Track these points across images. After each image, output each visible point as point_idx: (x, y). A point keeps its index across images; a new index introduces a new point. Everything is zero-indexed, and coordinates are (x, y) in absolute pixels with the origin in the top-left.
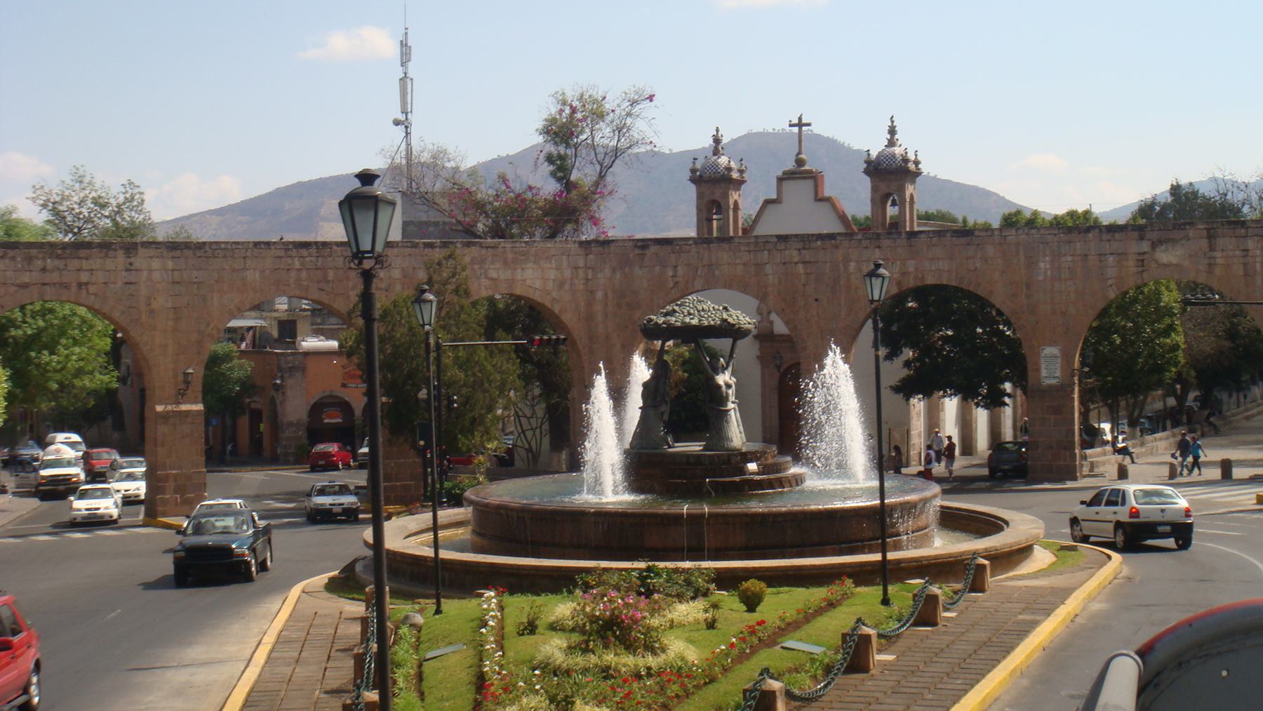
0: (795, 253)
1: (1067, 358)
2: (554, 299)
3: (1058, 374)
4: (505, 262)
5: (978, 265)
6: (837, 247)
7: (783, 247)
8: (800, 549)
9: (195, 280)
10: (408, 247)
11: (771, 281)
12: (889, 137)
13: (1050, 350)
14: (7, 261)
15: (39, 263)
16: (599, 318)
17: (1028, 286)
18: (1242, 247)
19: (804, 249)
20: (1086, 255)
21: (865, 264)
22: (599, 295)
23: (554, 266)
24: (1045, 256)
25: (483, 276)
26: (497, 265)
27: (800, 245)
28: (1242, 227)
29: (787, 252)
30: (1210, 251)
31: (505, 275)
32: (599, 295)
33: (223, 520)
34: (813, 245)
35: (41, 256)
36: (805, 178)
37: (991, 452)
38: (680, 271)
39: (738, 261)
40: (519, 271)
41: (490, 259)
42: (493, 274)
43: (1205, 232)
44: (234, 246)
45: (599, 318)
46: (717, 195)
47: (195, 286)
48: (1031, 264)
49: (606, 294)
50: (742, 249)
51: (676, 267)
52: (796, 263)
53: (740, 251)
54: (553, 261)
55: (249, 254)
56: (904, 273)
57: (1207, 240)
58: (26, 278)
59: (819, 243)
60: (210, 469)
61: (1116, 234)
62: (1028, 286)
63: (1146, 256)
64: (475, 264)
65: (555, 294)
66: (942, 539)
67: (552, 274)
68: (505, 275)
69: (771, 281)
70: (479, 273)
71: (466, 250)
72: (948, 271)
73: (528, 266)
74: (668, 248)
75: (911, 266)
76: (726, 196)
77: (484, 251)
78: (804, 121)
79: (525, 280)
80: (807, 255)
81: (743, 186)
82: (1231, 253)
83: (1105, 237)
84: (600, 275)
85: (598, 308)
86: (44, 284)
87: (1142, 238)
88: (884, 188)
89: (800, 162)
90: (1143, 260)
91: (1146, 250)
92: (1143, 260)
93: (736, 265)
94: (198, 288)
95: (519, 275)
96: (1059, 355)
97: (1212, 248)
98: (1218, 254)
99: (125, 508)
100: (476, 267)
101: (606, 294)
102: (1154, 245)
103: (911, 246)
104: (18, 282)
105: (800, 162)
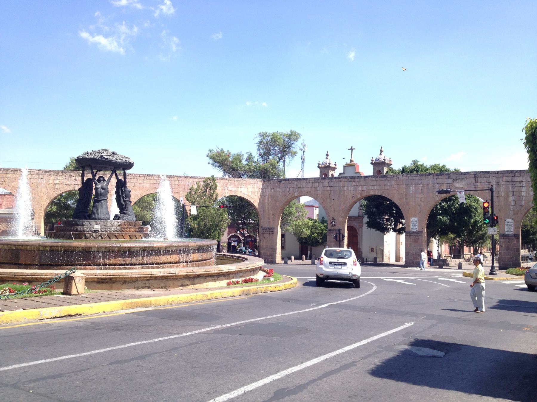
0: (327, 183)
1: (420, 222)
3: (417, 228)
4: (235, 185)
5: (388, 188)
6: (341, 181)
7: (323, 181)
8: (114, 267)
11: (319, 193)
13: (414, 219)
14: (63, 177)
15: (73, 178)
16: (266, 204)
17: (406, 195)
18: (488, 181)
19: (330, 182)
20: (428, 184)
21: (350, 187)
22: (267, 197)
23: (252, 187)
24: (412, 184)
26: (232, 186)
27: (329, 181)
28: (488, 174)
29: (324, 183)
30: (475, 182)
31: (234, 189)
32: (267, 197)
34: (333, 180)
35: (74, 175)
36: (352, 166)
38: (291, 189)
39: (309, 186)
40: (239, 188)
41: (229, 184)
42: (230, 189)
43: (473, 175)
44: (140, 175)
45: (266, 204)
46: (326, 172)
48: (408, 188)
49: (269, 197)
50: (310, 182)
51: (290, 188)
52: (327, 187)
53: (310, 183)
55: (145, 178)
56: (363, 190)
57: (474, 179)
58: (69, 182)
59: (335, 180)
61: (439, 176)
62: (406, 195)
63: (451, 185)
65: (252, 196)
67: (251, 190)
68: (234, 189)
69: (319, 193)
71: (221, 181)
72: (378, 190)
74: (288, 182)
75: (365, 188)
76: (329, 172)
77: (227, 181)
78: (353, 148)
80: (331, 184)
81: (336, 170)
82: (484, 184)
83: (435, 177)
84: (267, 191)
85: (266, 201)
86: (75, 185)
87: (449, 178)
88: (377, 169)
89: (351, 161)
90: (449, 186)
91: (450, 182)
92: (449, 186)
93: (308, 187)
95: (239, 189)
96: (417, 220)
97: (476, 182)
98: (479, 184)
100: (224, 186)
101: (269, 197)
102: (454, 181)
103: (365, 181)
104: (66, 183)
105: (351, 161)
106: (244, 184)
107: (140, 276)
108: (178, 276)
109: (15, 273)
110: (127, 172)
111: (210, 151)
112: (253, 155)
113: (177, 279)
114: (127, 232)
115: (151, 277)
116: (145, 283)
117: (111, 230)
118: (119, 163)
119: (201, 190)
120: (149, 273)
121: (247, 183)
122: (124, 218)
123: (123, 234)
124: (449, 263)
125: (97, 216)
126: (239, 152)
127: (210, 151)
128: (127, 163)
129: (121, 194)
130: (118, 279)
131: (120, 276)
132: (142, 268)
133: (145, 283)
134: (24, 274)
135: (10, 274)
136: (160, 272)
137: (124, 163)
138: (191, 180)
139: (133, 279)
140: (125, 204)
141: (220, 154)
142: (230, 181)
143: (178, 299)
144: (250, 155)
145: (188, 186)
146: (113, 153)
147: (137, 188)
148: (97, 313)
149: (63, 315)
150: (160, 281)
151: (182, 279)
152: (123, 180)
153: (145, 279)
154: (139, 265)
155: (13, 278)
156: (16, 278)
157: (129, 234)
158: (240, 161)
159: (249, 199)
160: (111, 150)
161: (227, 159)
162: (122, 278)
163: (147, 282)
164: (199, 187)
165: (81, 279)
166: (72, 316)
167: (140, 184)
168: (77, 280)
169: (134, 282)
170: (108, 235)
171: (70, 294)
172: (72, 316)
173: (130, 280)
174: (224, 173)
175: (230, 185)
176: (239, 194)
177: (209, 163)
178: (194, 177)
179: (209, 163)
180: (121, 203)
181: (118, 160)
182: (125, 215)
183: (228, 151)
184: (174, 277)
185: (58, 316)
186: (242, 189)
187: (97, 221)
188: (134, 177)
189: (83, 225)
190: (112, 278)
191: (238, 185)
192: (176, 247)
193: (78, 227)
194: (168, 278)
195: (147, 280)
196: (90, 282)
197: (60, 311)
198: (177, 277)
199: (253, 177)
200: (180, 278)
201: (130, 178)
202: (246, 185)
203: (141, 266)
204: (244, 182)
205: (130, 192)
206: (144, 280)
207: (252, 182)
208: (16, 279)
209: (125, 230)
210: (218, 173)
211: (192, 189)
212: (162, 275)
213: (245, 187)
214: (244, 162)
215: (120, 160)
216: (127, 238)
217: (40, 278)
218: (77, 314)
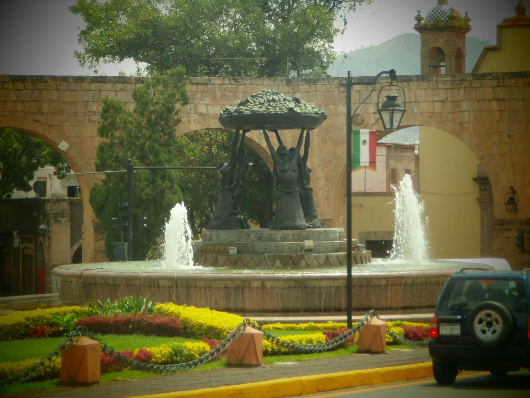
25: (192, 111)
26: (207, 101)
42: (202, 109)
138: (94, 86)
142: (201, 88)
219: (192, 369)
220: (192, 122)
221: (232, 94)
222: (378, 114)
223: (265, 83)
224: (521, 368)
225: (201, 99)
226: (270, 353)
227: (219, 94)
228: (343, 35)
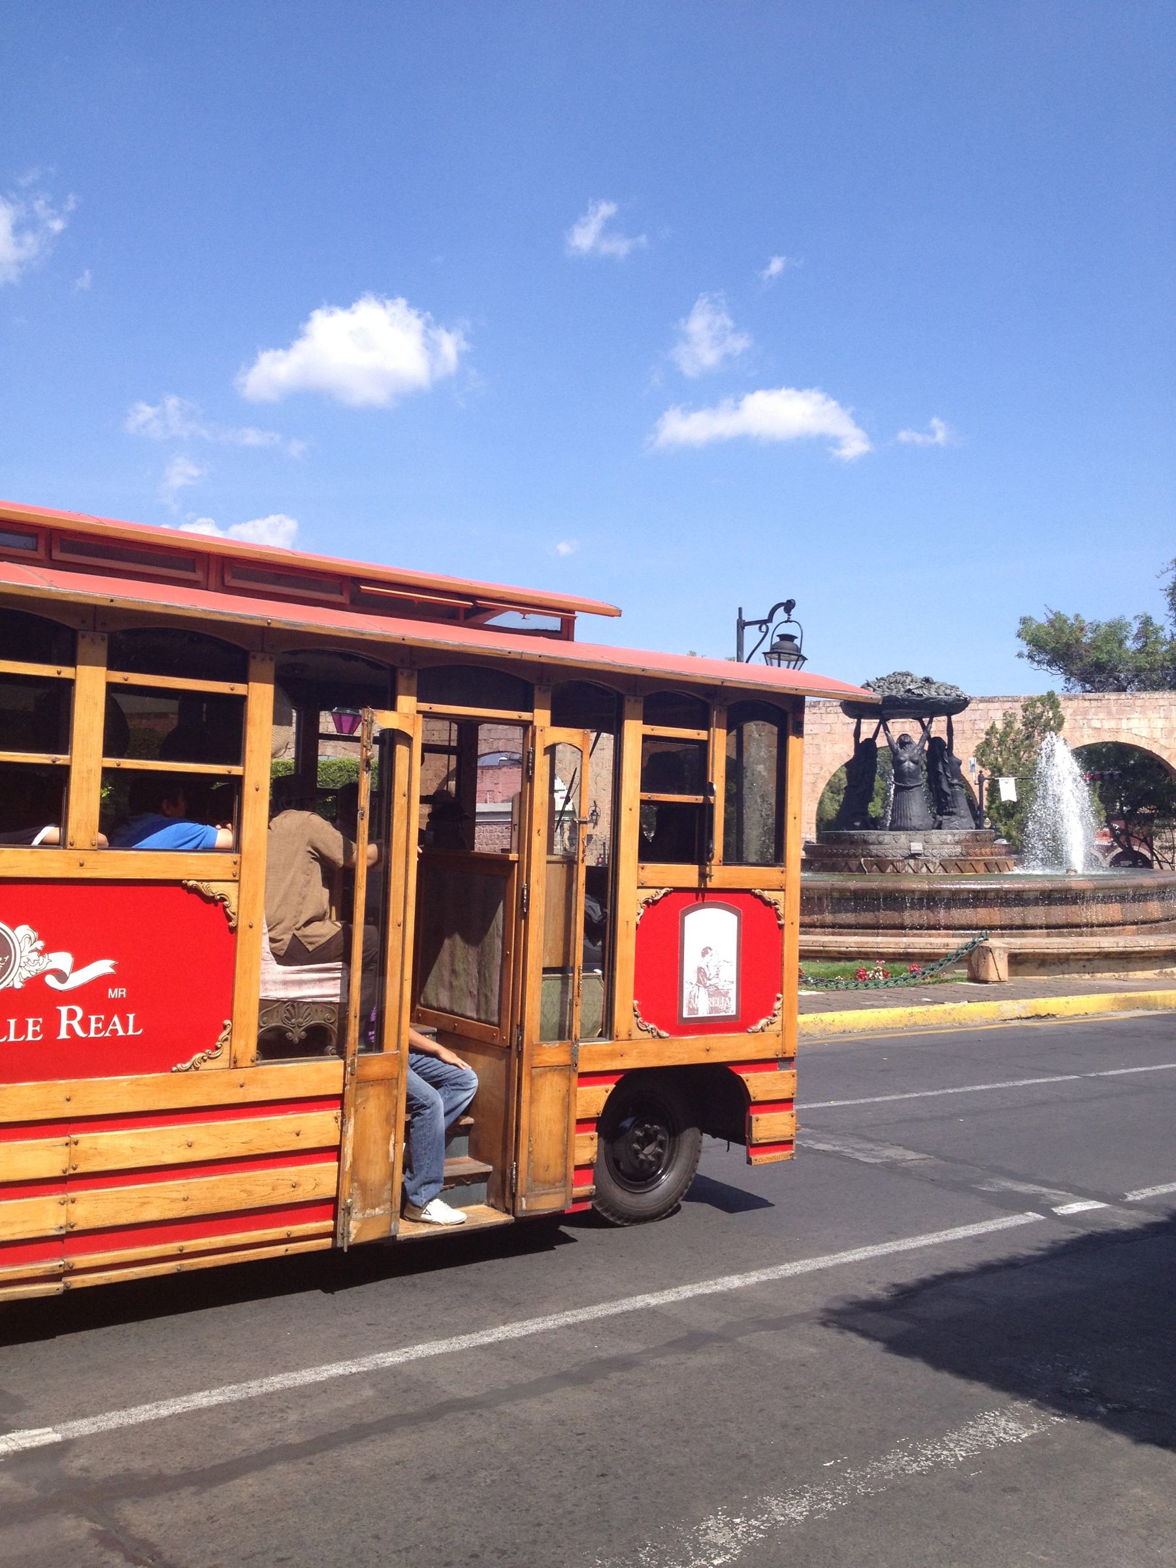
2: (1162, 746)
4: (1109, 713)
9: (811, 732)
10: (1008, 701)
12: (374, 718)
23: (1162, 716)
25: (1085, 726)
26: (1101, 716)
33: (577, 1200)
37: (112, 971)
40: (1124, 721)
42: (1097, 724)
47: (811, 737)
54: (1161, 711)
60: (567, 1035)
64: (1077, 715)
65: (1163, 742)
66: (598, 1152)
67: (1160, 723)
70: (1081, 724)
71: (1070, 703)
73: (1133, 716)
79: (1130, 729)
94: (813, 738)
99: (578, 1171)
100: (1078, 718)
106: (1138, 709)
107: (1075, 950)
108: (1155, 952)
109: (823, 942)
110: (954, 718)
111: (1024, 621)
112: (1157, 621)
113: (1149, 958)
114: (977, 856)
115: (1098, 953)
116: (1084, 966)
117: (944, 854)
118: (945, 702)
119: (1019, 732)
120: (1094, 945)
121: (1147, 704)
122: (952, 825)
123: (971, 860)
124: (306, 1030)
125: (908, 823)
126: (1117, 616)
127: (1024, 621)
128: (959, 700)
129: (941, 771)
130: (1030, 957)
131: (1036, 950)
132: (1048, 935)
133: (1084, 966)
134: (843, 945)
135: (814, 944)
136: (1118, 943)
137: (953, 702)
138: (981, 706)
139: (1062, 957)
140: (952, 792)
141: (1057, 622)
142: (1094, 703)
143: (913, 1020)
144: (1147, 622)
145: (974, 724)
146: (927, 680)
147: (837, 737)
148: (1077, 1015)
149: (1029, 1015)
150: (1116, 961)
151: (1160, 960)
152: (945, 738)
153: (1086, 957)
154: (1041, 928)
155: (820, 952)
156: (827, 952)
157: (984, 860)
158: (1121, 643)
159: (1156, 750)
160: (920, 674)
161: (1078, 640)
162: (1039, 954)
163: (1087, 964)
164: (1009, 724)
165: (1002, 952)
166: (1042, 1017)
167: (845, 727)
168: (996, 953)
169: (1062, 963)
170: (941, 864)
171: (986, 982)
172: (1042, 1017)
173: (1053, 959)
174: (1068, 679)
175: (1094, 714)
176: (1124, 739)
177: (1020, 655)
178: (990, 698)
179: (1020, 655)
180: (943, 790)
181: (943, 696)
182: (953, 818)
183: (1077, 616)
184: (1145, 955)
185: (1023, 1016)
186: (1133, 723)
187: (911, 832)
188: (829, 710)
189: (880, 843)
190: (1020, 954)
191: (1120, 712)
192: (1116, 888)
193: (871, 847)
194: (1132, 956)
195: (1089, 960)
196: (1017, 961)
197: (1025, 1008)
198: (1150, 955)
199: (1156, 686)
200: (1155, 957)
201: (818, 711)
202: (1143, 712)
203: (1046, 931)
204: (1139, 702)
205: (960, 763)
206: (1081, 959)
207: (1161, 702)
208: (824, 955)
209: (971, 851)
210: (1051, 680)
211: (992, 731)
212: (1121, 949)
213: (1142, 716)
214: (1130, 645)
215: (946, 695)
216: (981, 868)
217: (874, 953)
218: (1049, 1014)
219: (814, 1303)
220: (1086, 736)
221: (1129, 708)
222: (124, 711)
223: (1165, 696)
224: (311, 314)
225: (1096, 714)
226: (620, 1126)
227: (1114, 709)
228: (1017, 658)
